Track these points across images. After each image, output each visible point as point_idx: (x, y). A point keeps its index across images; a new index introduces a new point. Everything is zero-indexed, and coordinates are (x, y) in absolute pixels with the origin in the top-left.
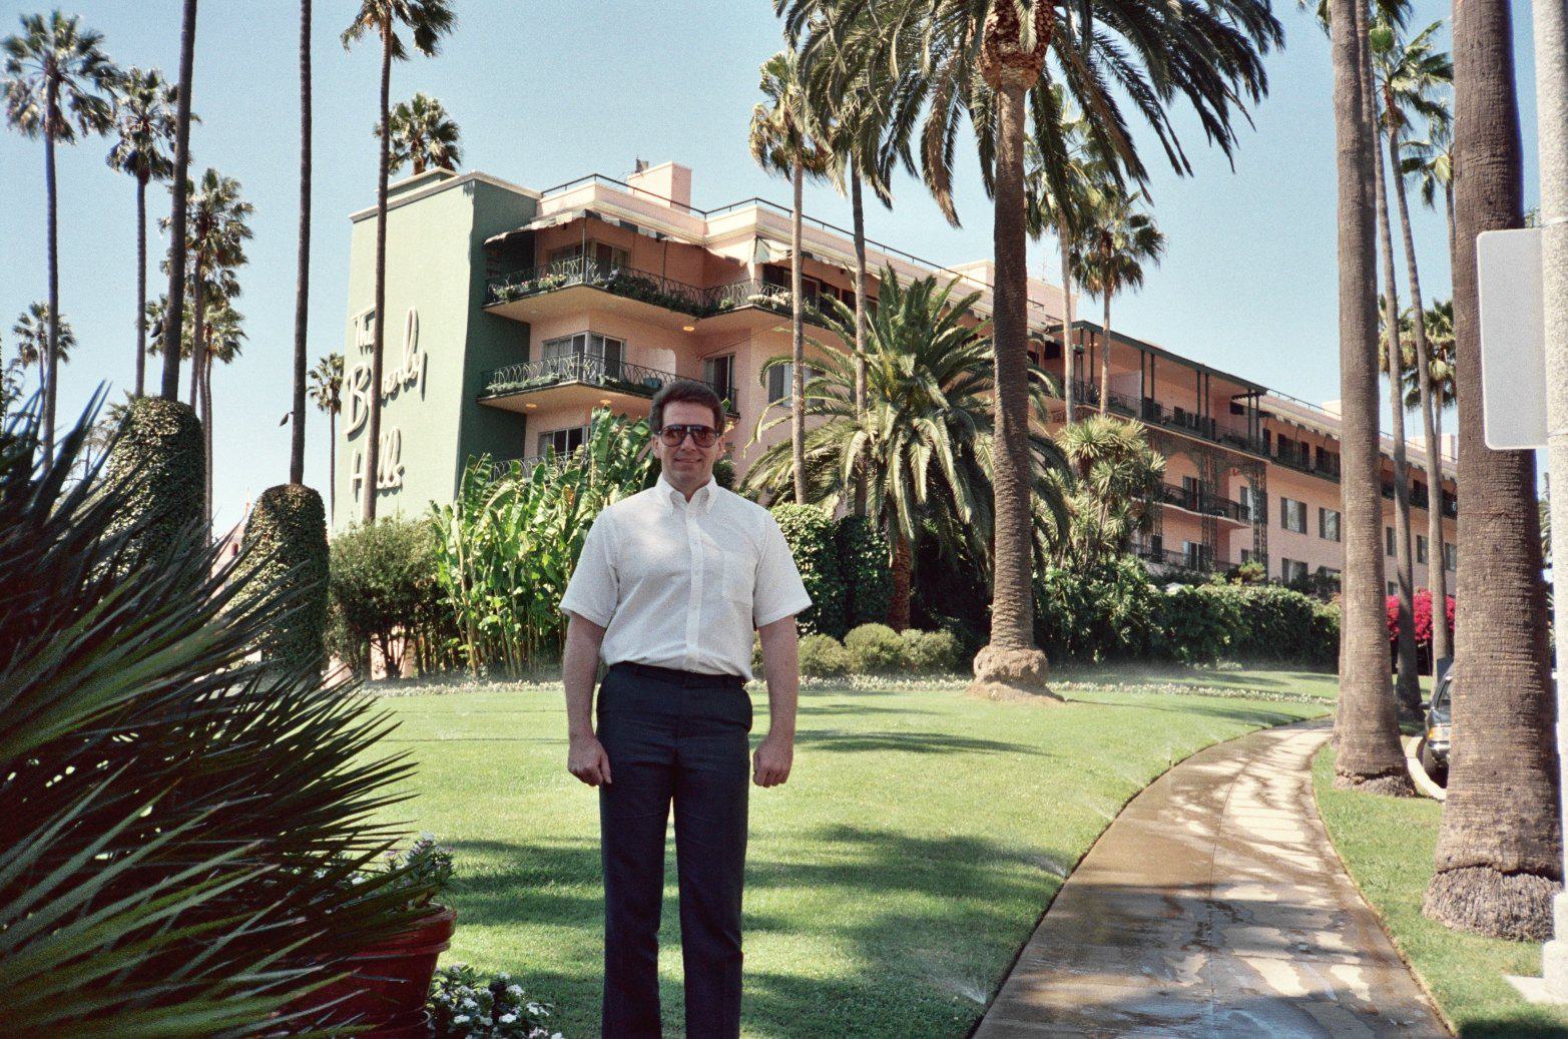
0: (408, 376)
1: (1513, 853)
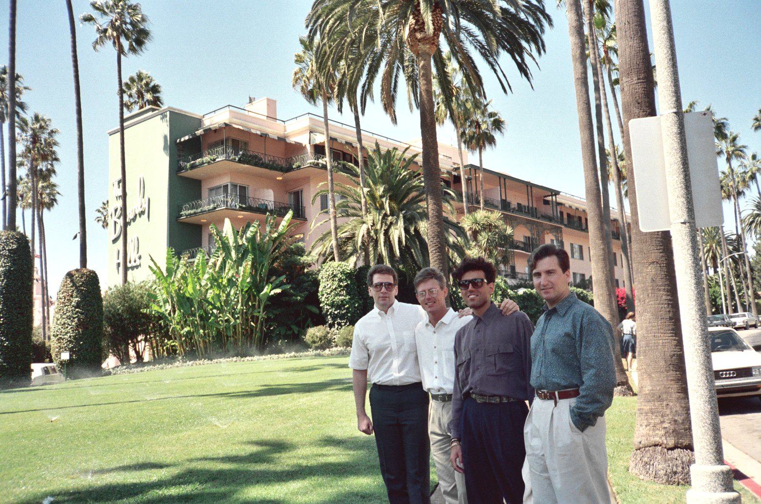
0: (141, 210)
1: (671, 438)
